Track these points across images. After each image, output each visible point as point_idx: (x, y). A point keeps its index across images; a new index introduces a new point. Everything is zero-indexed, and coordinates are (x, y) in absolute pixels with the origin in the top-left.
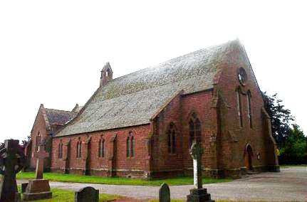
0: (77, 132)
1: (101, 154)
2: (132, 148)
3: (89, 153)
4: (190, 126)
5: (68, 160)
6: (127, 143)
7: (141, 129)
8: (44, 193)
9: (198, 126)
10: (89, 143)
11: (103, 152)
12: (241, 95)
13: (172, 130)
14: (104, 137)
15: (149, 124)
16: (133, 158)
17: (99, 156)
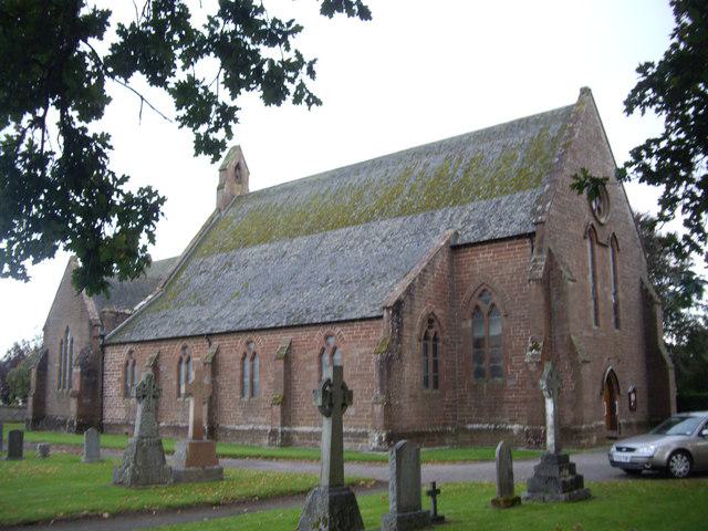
12: (596, 247)
15: (380, 317)
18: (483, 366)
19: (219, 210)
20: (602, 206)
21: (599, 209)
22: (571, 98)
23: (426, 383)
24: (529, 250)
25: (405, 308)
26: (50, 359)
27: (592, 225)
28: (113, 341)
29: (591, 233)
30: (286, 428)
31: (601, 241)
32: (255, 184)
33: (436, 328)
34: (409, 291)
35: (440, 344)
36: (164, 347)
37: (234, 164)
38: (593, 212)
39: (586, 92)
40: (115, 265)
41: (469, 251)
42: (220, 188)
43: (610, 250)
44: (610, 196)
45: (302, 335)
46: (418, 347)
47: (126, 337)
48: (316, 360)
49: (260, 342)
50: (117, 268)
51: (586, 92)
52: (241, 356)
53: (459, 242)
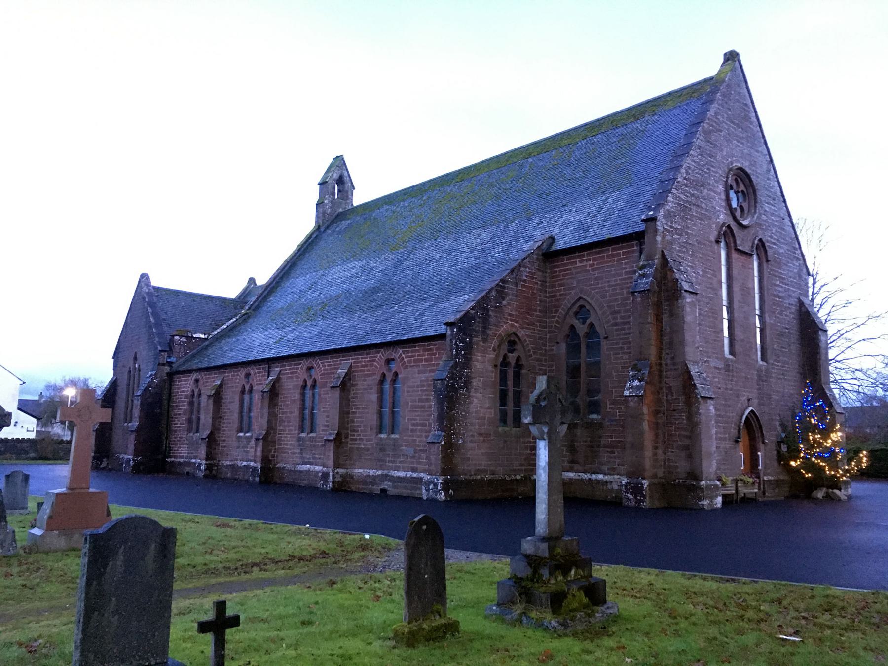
0: (240, 358)
1: (307, 422)
2: (394, 406)
3: (345, 414)
4: (568, 346)
5: (212, 441)
6: (381, 392)
7: (419, 352)
8: (215, 333)
9: (594, 347)
10: (274, 386)
11: (312, 415)
12: (735, 255)
13: (512, 357)
14: (316, 374)
15: (442, 337)
16: (311, 435)
17: (302, 430)
18: (578, 400)
19: (318, 229)
20: (745, 205)
21: (741, 207)
22: (710, 67)
23: (504, 420)
24: (637, 254)
25: (477, 326)
26: (119, 389)
27: (729, 227)
28: (181, 369)
29: (727, 235)
30: (341, 471)
31: (740, 248)
32: (359, 198)
33: (519, 351)
34: (482, 305)
35: (524, 372)
36: (229, 374)
37: (336, 176)
38: (732, 211)
39: (732, 57)
40: (793, 463)
41: (578, 263)
42: (319, 205)
43: (755, 257)
44: (759, 194)
45: (363, 358)
46: (493, 376)
47: (195, 364)
48: (375, 389)
49: (321, 366)
50: (796, 462)
51: (732, 57)
52: (301, 383)
53: (554, 248)
